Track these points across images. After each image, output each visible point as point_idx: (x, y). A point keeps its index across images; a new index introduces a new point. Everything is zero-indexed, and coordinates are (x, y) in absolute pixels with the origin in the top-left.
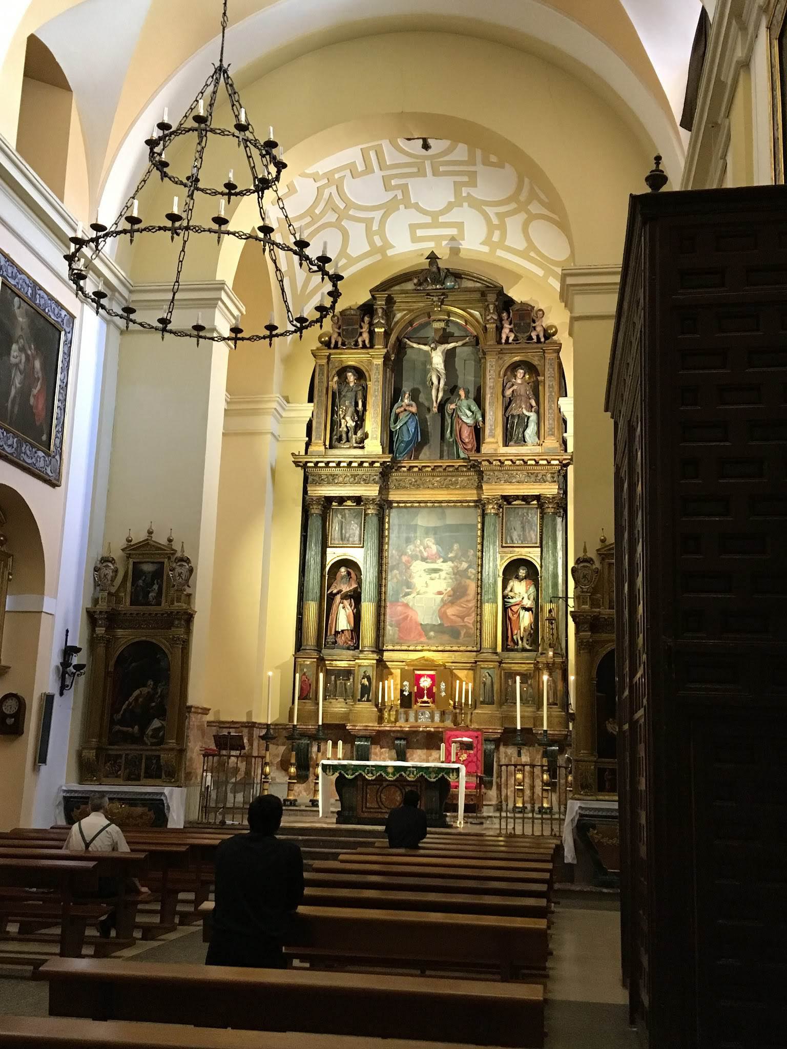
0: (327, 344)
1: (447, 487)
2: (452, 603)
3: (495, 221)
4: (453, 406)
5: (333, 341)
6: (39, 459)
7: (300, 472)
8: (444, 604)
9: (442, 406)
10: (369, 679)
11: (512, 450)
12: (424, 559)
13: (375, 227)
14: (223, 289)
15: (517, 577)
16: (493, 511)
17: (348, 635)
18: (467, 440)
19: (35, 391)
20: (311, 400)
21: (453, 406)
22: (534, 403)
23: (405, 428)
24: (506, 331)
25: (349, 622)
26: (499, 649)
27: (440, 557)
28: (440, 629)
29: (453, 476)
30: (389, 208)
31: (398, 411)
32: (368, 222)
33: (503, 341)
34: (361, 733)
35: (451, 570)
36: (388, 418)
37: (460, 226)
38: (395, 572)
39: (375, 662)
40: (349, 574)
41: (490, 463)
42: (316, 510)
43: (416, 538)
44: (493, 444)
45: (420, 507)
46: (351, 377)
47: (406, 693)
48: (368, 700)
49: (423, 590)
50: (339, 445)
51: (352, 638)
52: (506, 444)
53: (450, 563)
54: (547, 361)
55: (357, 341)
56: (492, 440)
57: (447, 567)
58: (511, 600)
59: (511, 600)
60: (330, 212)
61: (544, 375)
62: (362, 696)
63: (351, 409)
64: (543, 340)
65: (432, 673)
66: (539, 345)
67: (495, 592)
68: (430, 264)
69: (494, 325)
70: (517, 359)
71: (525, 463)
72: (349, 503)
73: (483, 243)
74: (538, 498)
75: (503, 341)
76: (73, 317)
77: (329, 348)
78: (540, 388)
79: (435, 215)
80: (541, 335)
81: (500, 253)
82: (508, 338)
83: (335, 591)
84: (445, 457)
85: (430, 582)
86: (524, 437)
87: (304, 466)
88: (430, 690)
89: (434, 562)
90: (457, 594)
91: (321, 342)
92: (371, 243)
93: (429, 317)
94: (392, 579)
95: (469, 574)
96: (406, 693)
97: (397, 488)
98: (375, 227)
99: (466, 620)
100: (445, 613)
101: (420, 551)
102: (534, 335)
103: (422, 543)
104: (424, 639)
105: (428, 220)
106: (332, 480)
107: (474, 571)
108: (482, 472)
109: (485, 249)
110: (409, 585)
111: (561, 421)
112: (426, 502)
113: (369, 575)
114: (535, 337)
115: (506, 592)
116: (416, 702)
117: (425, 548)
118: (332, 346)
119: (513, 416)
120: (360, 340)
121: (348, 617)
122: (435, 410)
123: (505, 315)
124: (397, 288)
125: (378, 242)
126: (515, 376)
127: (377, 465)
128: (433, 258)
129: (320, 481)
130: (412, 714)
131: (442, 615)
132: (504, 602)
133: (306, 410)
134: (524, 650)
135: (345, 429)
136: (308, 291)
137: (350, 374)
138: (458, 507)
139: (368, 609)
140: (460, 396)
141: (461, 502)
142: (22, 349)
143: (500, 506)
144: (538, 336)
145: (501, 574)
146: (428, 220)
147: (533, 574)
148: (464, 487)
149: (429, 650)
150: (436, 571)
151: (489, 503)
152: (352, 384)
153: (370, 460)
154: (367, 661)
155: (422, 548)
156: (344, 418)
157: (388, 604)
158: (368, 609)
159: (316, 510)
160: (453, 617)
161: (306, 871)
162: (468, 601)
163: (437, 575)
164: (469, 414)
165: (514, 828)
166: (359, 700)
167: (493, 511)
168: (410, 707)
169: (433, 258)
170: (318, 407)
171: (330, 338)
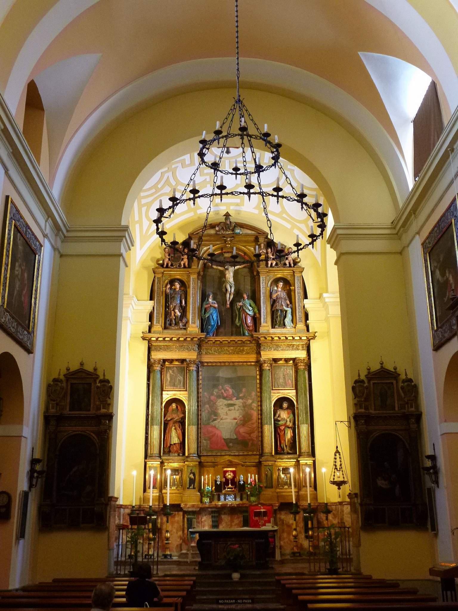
0: (162, 265)
1: (238, 353)
2: (243, 425)
4: (241, 304)
5: (166, 264)
6: (23, 336)
7: (146, 342)
9: (232, 303)
10: (194, 475)
11: (278, 331)
12: (225, 398)
14: (127, 230)
16: (267, 368)
18: (250, 324)
19: (24, 292)
20: (151, 298)
21: (241, 304)
22: (288, 303)
23: (211, 317)
25: (179, 438)
27: (235, 396)
29: (241, 346)
31: (207, 306)
33: (269, 266)
34: (190, 509)
36: (203, 310)
39: (197, 463)
41: (266, 338)
42: (157, 368)
44: (265, 326)
45: (221, 366)
46: (177, 285)
47: (218, 483)
48: (194, 488)
49: (225, 417)
50: (171, 327)
51: (181, 449)
52: (273, 327)
53: (241, 400)
55: (180, 264)
56: (265, 324)
57: (239, 402)
58: (280, 423)
59: (280, 423)
62: (190, 486)
63: (179, 305)
64: (292, 265)
65: (234, 469)
66: (291, 269)
67: (270, 417)
68: (226, 219)
71: (286, 338)
72: (177, 363)
73: (254, 208)
74: (294, 360)
75: (269, 266)
76: (41, 246)
77: (163, 267)
80: (292, 262)
82: (272, 264)
83: (169, 419)
85: (229, 412)
86: (284, 323)
87: (149, 341)
89: (232, 400)
90: (246, 419)
91: (158, 264)
93: (222, 250)
94: (205, 410)
96: (218, 483)
97: (206, 354)
99: (252, 435)
101: (222, 393)
102: (287, 262)
103: (223, 388)
104: (226, 448)
106: (277, 348)
108: (260, 344)
110: (216, 414)
114: (288, 264)
115: (276, 418)
116: (225, 488)
117: (225, 391)
118: (165, 266)
119: (277, 310)
120: (182, 263)
122: (228, 306)
123: (269, 250)
126: (277, 287)
127: (195, 339)
128: (227, 215)
129: (159, 349)
130: (222, 497)
131: (237, 433)
133: (149, 305)
134: (288, 453)
137: (177, 283)
138: (240, 365)
140: (244, 298)
141: (246, 362)
142: (20, 266)
143: (271, 365)
144: (289, 263)
148: (248, 353)
149: (230, 455)
151: (265, 363)
153: (192, 337)
155: (223, 391)
156: (174, 310)
159: (157, 368)
160: (243, 434)
161: (438, 581)
162: (253, 424)
163: (232, 408)
164: (250, 308)
165: (320, 568)
166: (188, 488)
167: (267, 368)
168: (221, 491)
169: (227, 215)
170: (159, 302)
171: (163, 261)
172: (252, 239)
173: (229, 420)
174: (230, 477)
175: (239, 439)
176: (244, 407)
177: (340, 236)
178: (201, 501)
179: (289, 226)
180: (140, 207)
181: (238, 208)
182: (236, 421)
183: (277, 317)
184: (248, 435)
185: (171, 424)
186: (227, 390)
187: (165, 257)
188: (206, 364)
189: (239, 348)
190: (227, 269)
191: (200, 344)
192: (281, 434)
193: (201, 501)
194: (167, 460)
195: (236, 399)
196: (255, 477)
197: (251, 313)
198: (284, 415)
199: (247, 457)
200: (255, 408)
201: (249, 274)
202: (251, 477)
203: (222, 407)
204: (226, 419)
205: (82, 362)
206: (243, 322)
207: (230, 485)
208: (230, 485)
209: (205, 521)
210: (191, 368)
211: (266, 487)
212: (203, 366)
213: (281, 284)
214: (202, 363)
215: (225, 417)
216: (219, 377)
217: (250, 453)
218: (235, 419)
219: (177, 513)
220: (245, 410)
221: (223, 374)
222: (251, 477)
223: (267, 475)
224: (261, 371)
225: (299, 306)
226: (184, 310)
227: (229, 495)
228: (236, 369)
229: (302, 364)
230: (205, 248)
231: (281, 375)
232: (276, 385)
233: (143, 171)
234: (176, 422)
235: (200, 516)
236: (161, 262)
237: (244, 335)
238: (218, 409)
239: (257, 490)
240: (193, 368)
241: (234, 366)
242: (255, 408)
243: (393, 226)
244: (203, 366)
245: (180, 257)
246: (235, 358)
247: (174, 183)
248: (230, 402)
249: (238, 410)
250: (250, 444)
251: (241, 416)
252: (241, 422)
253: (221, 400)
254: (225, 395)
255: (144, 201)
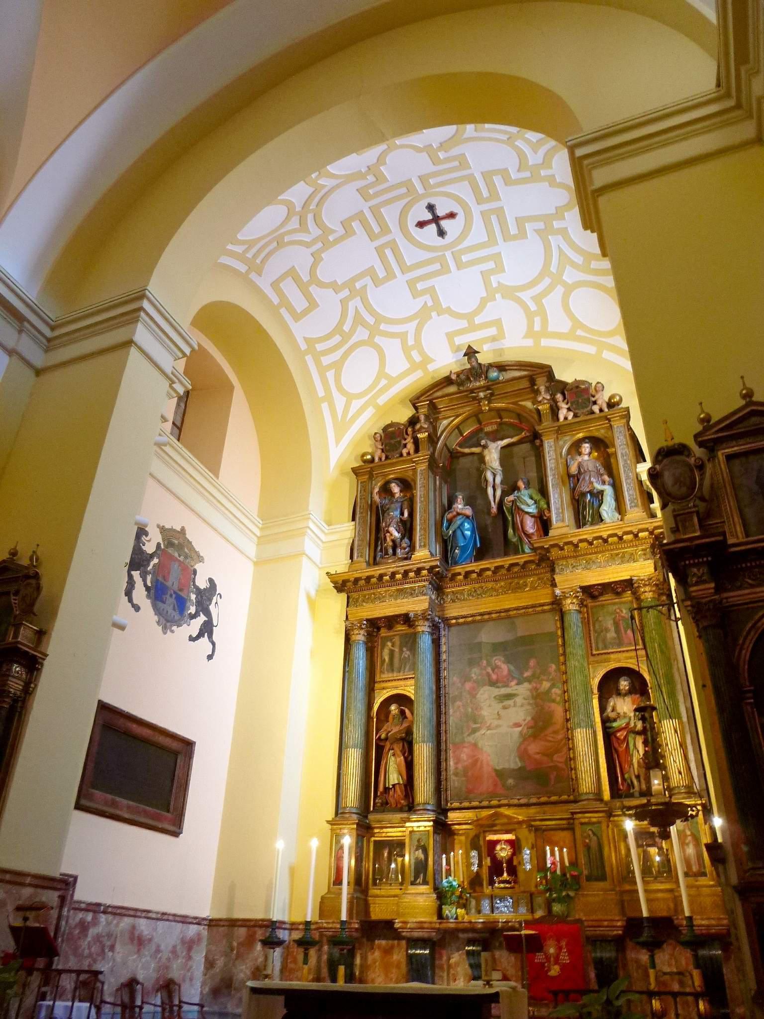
3: (533, 307)
8: (525, 739)
10: (425, 851)
12: (493, 684)
13: (411, 342)
15: (619, 694)
17: (399, 792)
20: (354, 519)
23: (459, 533)
24: (562, 414)
26: (607, 795)
27: (513, 678)
28: (522, 774)
30: (423, 316)
32: (403, 336)
35: (528, 693)
37: (498, 323)
38: (458, 703)
40: (402, 713)
43: (481, 658)
46: (396, 489)
48: (425, 882)
53: (526, 685)
54: (615, 430)
56: (560, 524)
57: (523, 690)
59: (615, 725)
60: (360, 328)
61: (614, 446)
69: (548, 405)
70: (581, 435)
73: (525, 337)
78: (612, 460)
79: (469, 317)
81: (544, 342)
84: (691, 880)
85: (503, 713)
86: (600, 516)
88: (510, 861)
89: (507, 686)
90: (540, 724)
92: (409, 358)
95: (554, 696)
97: (454, 601)
98: (411, 342)
99: (555, 757)
100: (526, 750)
101: (489, 675)
102: (596, 409)
103: (489, 664)
105: (464, 324)
107: (559, 692)
109: (529, 342)
111: (646, 496)
112: (489, 613)
113: (423, 712)
117: (493, 670)
119: (584, 494)
120: (405, 451)
121: (399, 766)
124: (439, 394)
125: (417, 357)
126: (580, 454)
127: (425, 572)
130: (486, 905)
131: (523, 754)
132: (605, 729)
135: (391, 544)
136: (349, 416)
139: (423, 752)
141: (533, 606)
145: (595, 691)
146: (464, 324)
147: (639, 686)
148: (534, 588)
150: (509, 696)
152: (397, 495)
154: (422, 824)
155: (489, 670)
157: (450, 746)
158: (423, 752)
160: (537, 757)
162: (555, 732)
163: (511, 702)
164: (530, 502)
172: (525, 384)
173: (504, 729)
174: (503, 854)
175: (528, 769)
176: (535, 698)
177: (586, 162)
178: (440, 915)
179: (591, 349)
180: (322, 371)
181: (496, 345)
182: (520, 729)
183: (584, 508)
184: (545, 759)
185: (388, 745)
186: (497, 667)
187: (377, 448)
188: (454, 621)
189: (514, 577)
190: (485, 447)
191: (439, 581)
192: (620, 750)
193: (440, 915)
194: (379, 821)
195: (517, 684)
196: (561, 851)
197: (532, 509)
198: (624, 706)
199: (547, 808)
200: (558, 699)
201: (532, 453)
202: (553, 854)
203: (488, 702)
204: (498, 726)
205: (15, 548)
206: (520, 530)
207: (505, 874)
208: (505, 874)
209: (457, 964)
210: (420, 629)
211: (589, 879)
212: (450, 626)
213: (586, 447)
214: (446, 620)
215: (496, 722)
216: (480, 643)
217: (554, 798)
218: (517, 725)
219: (396, 942)
220: (537, 705)
221: (488, 635)
222: (553, 854)
223: (588, 847)
224: (562, 615)
225: (627, 478)
226: (407, 529)
227: (502, 899)
228: (513, 623)
229: (647, 589)
230: (445, 422)
231: (610, 624)
232: (601, 645)
233: (198, 207)
234: (397, 740)
235: (444, 952)
236: (369, 457)
237: (524, 552)
238: (481, 709)
239: (566, 883)
240: (423, 628)
241: (509, 617)
242: (558, 699)
243: (722, 92)
244: (450, 626)
245: (400, 442)
246: (510, 601)
247: (371, 320)
248: (504, 691)
249: (522, 706)
250: (552, 777)
251: (529, 718)
252: (530, 731)
253: (487, 688)
254: (494, 677)
255: (326, 360)
